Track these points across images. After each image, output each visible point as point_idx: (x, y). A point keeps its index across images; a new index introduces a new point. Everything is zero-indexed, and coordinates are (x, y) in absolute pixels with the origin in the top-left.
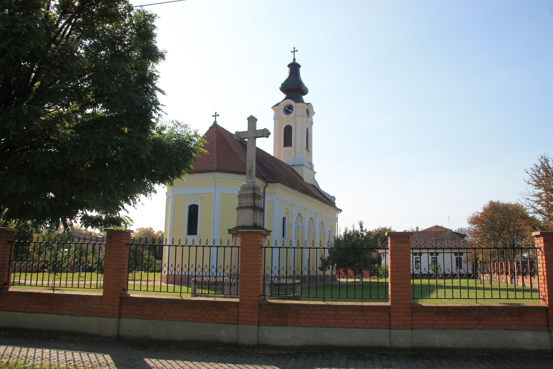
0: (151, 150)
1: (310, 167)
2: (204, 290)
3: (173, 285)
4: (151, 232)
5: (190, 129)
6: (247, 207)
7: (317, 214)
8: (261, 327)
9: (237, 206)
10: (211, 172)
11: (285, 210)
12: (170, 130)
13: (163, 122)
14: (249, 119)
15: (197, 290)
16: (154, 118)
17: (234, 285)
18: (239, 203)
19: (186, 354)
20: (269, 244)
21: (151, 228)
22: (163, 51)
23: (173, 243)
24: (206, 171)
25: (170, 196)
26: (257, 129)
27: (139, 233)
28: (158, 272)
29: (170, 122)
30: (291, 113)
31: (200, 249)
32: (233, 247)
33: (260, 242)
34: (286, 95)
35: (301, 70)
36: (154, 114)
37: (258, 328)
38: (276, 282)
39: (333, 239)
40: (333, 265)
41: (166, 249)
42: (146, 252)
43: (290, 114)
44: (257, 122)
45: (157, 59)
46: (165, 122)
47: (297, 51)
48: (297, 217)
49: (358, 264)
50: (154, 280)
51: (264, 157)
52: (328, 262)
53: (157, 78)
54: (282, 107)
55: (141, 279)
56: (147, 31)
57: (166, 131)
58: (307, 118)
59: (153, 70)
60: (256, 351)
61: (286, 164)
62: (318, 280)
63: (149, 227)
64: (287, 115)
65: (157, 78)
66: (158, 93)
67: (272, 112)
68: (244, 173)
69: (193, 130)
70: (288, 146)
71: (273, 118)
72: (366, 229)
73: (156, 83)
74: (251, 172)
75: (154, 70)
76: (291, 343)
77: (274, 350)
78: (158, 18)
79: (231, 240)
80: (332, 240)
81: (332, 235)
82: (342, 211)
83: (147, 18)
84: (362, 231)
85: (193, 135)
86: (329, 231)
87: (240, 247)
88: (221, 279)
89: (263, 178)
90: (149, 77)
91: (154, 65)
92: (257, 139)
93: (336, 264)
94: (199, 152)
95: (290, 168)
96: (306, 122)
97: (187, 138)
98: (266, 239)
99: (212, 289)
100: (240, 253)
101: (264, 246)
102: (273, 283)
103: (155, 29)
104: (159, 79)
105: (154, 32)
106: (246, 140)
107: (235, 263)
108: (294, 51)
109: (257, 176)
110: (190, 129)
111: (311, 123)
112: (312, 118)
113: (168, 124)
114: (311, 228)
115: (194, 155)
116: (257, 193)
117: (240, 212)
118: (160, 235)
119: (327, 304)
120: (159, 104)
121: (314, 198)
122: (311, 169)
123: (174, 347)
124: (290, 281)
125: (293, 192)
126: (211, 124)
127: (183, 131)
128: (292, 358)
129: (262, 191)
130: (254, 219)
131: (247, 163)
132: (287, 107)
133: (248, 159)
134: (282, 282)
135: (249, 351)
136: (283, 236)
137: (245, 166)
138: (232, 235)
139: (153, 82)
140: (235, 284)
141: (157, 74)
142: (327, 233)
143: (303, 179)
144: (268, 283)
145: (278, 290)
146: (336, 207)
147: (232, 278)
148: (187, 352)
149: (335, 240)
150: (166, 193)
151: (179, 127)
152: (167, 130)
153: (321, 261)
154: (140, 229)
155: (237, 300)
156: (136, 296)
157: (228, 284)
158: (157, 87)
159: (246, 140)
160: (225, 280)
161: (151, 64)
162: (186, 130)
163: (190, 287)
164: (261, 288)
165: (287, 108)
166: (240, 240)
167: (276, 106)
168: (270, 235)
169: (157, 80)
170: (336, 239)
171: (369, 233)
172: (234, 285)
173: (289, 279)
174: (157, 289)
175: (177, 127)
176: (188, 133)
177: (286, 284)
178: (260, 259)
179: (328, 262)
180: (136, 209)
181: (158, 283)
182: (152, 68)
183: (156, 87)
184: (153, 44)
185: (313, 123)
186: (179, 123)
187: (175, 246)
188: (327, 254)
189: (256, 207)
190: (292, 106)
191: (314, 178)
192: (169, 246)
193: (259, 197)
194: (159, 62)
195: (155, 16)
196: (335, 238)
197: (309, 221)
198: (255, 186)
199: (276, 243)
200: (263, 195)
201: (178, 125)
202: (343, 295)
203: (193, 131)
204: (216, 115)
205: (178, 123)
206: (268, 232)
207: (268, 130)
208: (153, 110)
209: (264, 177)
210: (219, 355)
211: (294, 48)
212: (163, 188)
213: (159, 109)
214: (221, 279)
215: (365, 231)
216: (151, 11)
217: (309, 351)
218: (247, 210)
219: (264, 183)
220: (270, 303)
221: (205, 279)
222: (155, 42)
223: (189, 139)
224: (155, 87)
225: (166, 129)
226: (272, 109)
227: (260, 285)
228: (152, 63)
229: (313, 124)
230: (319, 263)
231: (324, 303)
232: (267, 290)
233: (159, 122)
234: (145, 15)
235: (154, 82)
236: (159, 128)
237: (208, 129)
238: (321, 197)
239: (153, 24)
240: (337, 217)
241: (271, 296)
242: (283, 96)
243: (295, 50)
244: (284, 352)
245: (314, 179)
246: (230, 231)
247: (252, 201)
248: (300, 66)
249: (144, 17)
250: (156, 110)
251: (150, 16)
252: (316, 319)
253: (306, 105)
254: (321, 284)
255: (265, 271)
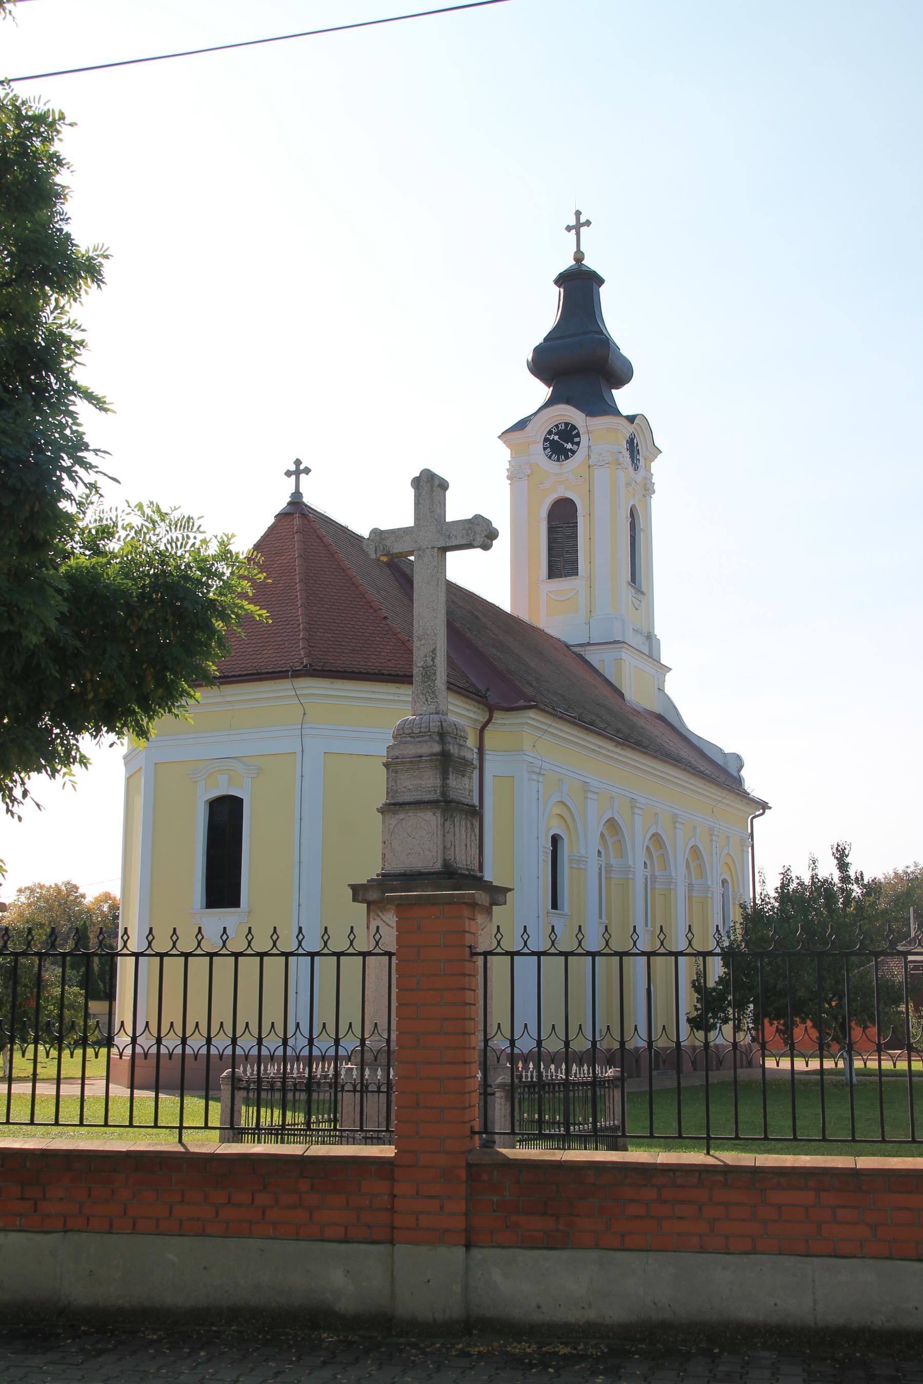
0: (62, 613)
1: (645, 650)
2: (269, 1111)
3: (153, 1094)
4: (71, 898)
5: (203, 532)
6: (418, 804)
7: (675, 822)
8: (477, 1253)
9: (382, 799)
10: (287, 677)
11: (557, 810)
12: (129, 538)
13: (107, 509)
14: (417, 483)
15: (244, 1108)
16: (69, 497)
17: (379, 1091)
18: (387, 788)
19: (199, 1364)
20: (499, 942)
21: (74, 882)
22: (95, 250)
23: (150, 943)
24: (267, 673)
25: (141, 768)
26: (449, 519)
27: (30, 905)
28: (99, 1044)
29: (129, 510)
30: (573, 452)
31: (249, 965)
32: (370, 954)
33: (467, 935)
34: (551, 388)
35: (605, 294)
36: (67, 485)
37: (466, 1252)
38: (532, 1077)
39: (739, 911)
40: (740, 1006)
41: (125, 967)
42: (52, 973)
43: (567, 458)
44: (447, 492)
45: (74, 282)
46: (113, 510)
47: (588, 223)
48: (602, 834)
49: (834, 1004)
50: (83, 1078)
51: (477, 618)
52: (722, 996)
53: (77, 351)
54: (538, 431)
55: (35, 1073)
56: (32, 176)
57: (115, 540)
58: (631, 469)
59: (58, 322)
60: (460, 1346)
61: (559, 640)
62: (687, 1065)
63: (65, 880)
64: (558, 460)
65: (77, 351)
66: (80, 406)
67: (503, 454)
68: (405, 678)
69: (216, 537)
70: (565, 576)
71: (506, 473)
72: (862, 874)
73: (72, 367)
74: (429, 673)
75: (63, 322)
76: (591, 1315)
77: (526, 1342)
78: (71, 125)
79: (361, 931)
80: (736, 916)
81: (734, 899)
82: (770, 808)
83: (31, 128)
84: (845, 879)
85: (214, 557)
86: (724, 882)
87: (393, 954)
88: (328, 1068)
89: (475, 694)
90: (47, 348)
91: (62, 302)
92: (448, 553)
93: (751, 1006)
94: (237, 615)
95: (574, 653)
96: (628, 484)
97: (191, 568)
98: (491, 918)
99: (297, 1104)
100: (394, 990)
101: (479, 950)
102: (520, 1081)
103: (64, 171)
104: (83, 356)
105: (58, 179)
106: (412, 558)
107: (377, 1012)
108: (578, 226)
109: (452, 687)
110: (203, 532)
111: (648, 489)
112: (648, 469)
113: (124, 516)
114: (657, 873)
115: (219, 625)
116: (452, 751)
117: (393, 821)
118: (105, 909)
119: (720, 1163)
120: (86, 447)
121: (665, 762)
122: (650, 656)
123: (155, 1337)
124: (580, 1073)
125: (588, 741)
126: (281, 502)
127: (177, 538)
128: (594, 1373)
129: (471, 742)
130: (445, 847)
131: (416, 644)
132: (555, 434)
133: (417, 630)
134: (552, 1076)
135: (435, 1344)
136: (555, 906)
137: (410, 652)
138: (365, 905)
139: (62, 366)
140: (379, 1088)
141: (76, 336)
142: (718, 890)
143: (621, 695)
144: (499, 1080)
145: (536, 1107)
146: (744, 796)
147: (369, 1065)
148: (202, 1354)
149: (746, 917)
150: (125, 758)
151: (162, 528)
152: (119, 540)
153: (696, 995)
154: (32, 891)
155: (388, 1151)
156: (17, 1145)
157: (355, 1086)
158: (79, 383)
159: (412, 558)
160: (343, 1072)
161: (53, 298)
162: (188, 537)
163: (217, 1100)
164: (474, 1106)
165: (556, 438)
166: (394, 925)
167: (514, 431)
168: (505, 903)
169: (76, 358)
170: (749, 911)
171: (873, 889)
172: (379, 1091)
173: (580, 1065)
174: (94, 1113)
175: (154, 529)
176: (197, 546)
177: (566, 1083)
178: (469, 996)
179: (722, 996)
180: (20, 819)
181: (96, 1088)
182: (55, 315)
183: (74, 384)
184: (57, 226)
185: (655, 487)
186: (163, 511)
187: (157, 954)
188: (716, 969)
189: (451, 802)
190: (574, 427)
191: (661, 690)
192: (137, 955)
193: (463, 766)
194: (82, 292)
195: (59, 120)
196: (743, 907)
197: (648, 847)
198: (444, 724)
199: (525, 937)
200: (475, 756)
201: (158, 519)
202: (780, 1123)
203: (214, 539)
204: (298, 471)
205: (159, 510)
206: (498, 894)
207: (488, 523)
208: (63, 469)
209: (480, 691)
210: (324, 1363)
211: (578, 214)
212: (111, 745)
213: (87, 466)
214: (328, 1068)
215: (857, 883)
216: (43, 101)
217: (659, 1346)
218: (419, 814)
219: (479, 711)
220: (509, 1159)
221: (272, 1070)
222: (61, 220)
223: (200, 569)
224: (69, 383)
225: (117, 536)
226: (500, 442)
227: (470, 1092)
228: (55, 295)
229: (654, 492)
230: (688, 1002)
231: (710, 1160)
232: (497, 1106)
233: (90, 512)
234: (19, 117)
235: (67, 364)
236: (90, 532)
237: (271, 521)
238: (691, 759)
239: (52, 151)
240: (749, 831)
241: (513, 1133)
242: (541, 392)
243: (583, 220)
244: (564, 1350)
245: (663, 691)
246: (358, 892)
247: (438, 782)
248: (600, 281)
249: (18, 126)
250: (77, 468)
251: (40, 119)
252: (681, 1218)
253: (626, 423)
254: (697, 1080)
255: (486, 1041)
